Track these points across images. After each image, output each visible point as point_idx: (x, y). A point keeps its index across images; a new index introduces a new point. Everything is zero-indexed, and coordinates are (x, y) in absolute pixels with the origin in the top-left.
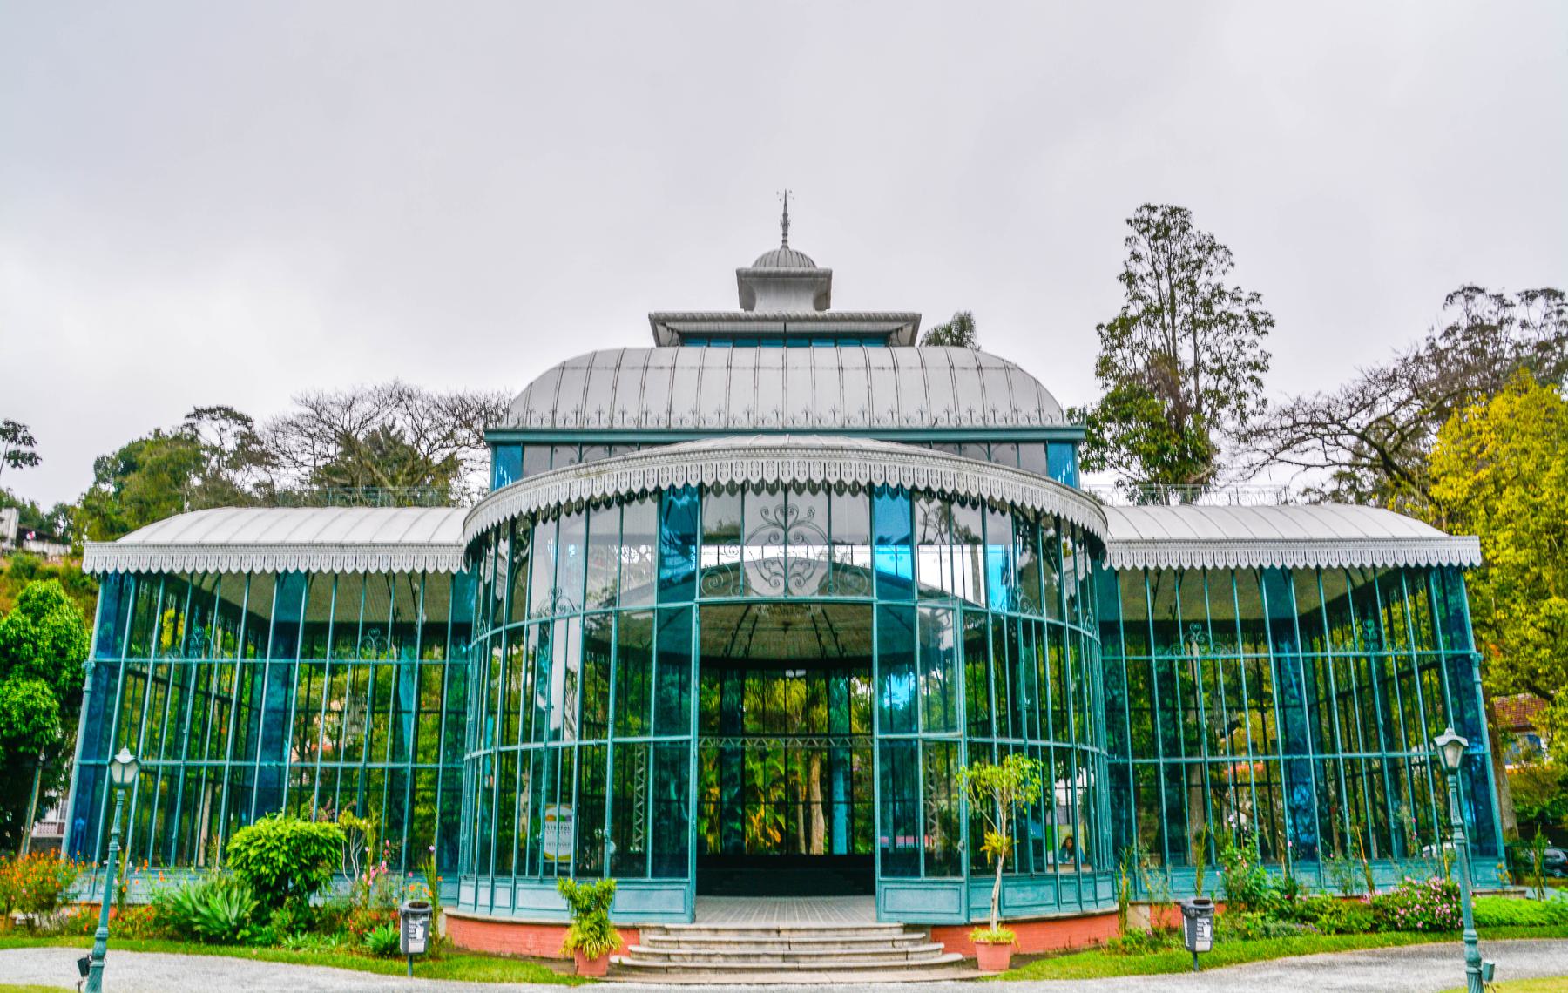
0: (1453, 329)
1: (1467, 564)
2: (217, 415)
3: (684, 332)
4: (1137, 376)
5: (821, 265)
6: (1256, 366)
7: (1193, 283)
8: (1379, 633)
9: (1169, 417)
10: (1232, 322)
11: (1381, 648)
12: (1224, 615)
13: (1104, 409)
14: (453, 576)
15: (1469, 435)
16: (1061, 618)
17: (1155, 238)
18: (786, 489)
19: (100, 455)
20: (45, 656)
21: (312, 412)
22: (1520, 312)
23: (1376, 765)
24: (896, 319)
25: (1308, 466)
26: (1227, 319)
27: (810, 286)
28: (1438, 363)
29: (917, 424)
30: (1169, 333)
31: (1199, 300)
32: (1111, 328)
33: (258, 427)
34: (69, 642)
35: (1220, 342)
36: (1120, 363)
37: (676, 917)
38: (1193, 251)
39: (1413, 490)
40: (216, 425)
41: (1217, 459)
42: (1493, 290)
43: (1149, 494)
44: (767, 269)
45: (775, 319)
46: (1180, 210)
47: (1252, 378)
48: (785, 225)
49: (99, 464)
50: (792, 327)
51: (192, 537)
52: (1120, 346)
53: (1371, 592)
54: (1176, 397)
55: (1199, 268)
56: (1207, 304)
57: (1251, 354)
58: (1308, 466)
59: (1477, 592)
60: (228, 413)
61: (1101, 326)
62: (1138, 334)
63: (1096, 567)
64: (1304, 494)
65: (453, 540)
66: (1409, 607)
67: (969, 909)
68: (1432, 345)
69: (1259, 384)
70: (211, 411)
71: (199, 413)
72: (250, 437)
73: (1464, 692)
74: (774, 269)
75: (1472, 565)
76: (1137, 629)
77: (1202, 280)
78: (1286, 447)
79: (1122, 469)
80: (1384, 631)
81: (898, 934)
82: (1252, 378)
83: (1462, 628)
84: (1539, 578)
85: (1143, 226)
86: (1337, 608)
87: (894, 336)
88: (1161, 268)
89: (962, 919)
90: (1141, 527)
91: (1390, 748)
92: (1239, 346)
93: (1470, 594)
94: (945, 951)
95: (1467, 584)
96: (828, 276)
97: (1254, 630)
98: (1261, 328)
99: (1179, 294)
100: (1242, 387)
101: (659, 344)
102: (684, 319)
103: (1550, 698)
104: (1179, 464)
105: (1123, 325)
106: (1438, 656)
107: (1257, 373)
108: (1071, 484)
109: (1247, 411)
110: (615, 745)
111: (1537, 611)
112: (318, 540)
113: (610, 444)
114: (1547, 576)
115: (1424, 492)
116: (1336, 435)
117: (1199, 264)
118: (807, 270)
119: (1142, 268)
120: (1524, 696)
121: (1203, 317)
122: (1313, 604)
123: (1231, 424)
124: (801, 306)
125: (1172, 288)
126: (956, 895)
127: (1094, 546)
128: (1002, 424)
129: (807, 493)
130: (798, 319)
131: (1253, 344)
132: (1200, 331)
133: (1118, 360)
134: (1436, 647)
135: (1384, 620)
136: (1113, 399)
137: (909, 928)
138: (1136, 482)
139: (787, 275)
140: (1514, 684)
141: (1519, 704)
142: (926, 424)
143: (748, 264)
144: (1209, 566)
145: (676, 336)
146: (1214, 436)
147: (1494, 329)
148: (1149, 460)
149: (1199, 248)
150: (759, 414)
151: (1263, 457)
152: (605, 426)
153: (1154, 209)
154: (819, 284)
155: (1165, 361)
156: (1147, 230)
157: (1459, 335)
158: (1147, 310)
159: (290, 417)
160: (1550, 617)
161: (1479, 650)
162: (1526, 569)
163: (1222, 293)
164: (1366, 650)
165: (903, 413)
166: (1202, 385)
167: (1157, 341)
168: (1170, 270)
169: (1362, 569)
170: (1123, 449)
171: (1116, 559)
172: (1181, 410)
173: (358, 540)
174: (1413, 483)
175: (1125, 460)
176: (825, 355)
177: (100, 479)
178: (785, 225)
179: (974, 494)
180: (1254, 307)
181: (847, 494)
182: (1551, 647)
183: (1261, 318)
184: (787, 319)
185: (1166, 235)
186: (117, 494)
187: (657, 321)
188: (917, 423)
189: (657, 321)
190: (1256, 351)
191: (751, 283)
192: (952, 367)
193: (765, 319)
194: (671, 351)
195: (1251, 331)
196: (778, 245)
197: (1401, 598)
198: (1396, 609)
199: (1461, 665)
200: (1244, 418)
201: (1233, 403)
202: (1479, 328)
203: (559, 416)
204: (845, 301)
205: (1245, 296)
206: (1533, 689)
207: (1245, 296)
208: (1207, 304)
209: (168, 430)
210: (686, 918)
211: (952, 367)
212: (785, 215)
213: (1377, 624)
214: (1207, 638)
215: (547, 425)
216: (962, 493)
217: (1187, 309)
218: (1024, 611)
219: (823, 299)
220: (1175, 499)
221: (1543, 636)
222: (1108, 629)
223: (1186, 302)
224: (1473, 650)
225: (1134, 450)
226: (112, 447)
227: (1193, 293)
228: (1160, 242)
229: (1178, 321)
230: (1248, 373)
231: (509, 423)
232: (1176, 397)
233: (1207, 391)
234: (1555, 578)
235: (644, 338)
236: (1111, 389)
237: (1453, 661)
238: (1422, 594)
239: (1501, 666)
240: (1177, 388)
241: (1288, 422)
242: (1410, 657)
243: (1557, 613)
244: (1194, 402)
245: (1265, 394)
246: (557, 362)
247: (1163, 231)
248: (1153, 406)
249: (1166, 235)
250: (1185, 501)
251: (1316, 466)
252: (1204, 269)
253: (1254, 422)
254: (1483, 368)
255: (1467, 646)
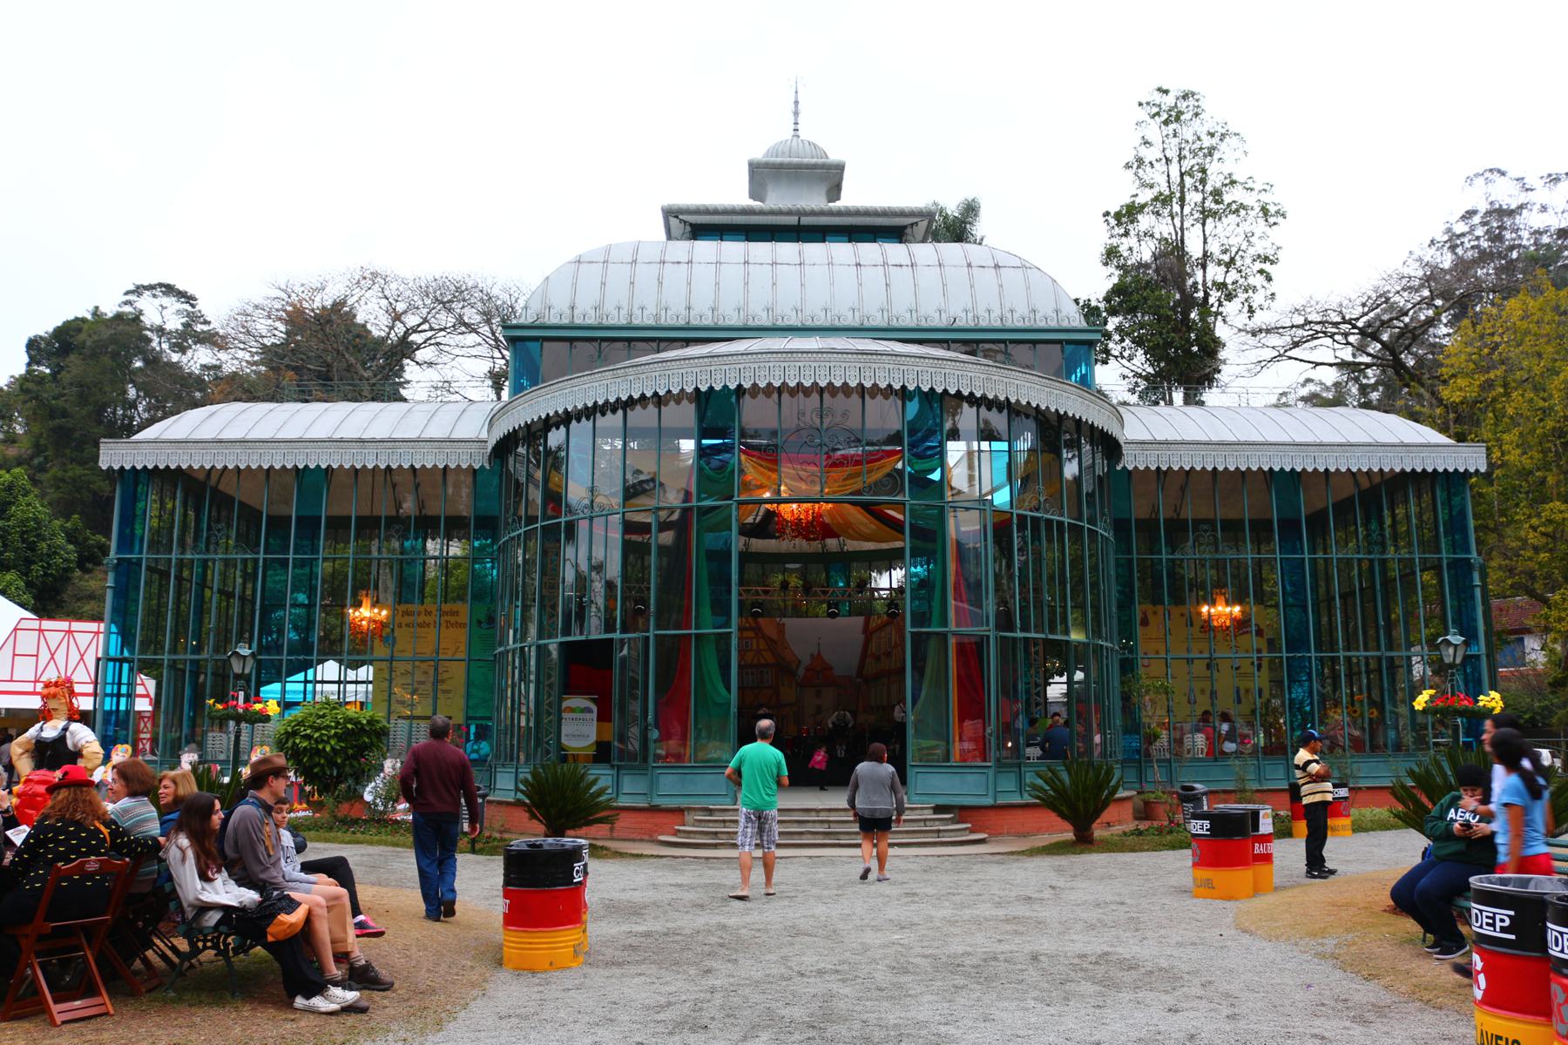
0: (1471, 213)
1: (1472, 470)
2: (158, 292)
3: (702, 226)
4: (1141, 265)
5: (834, 157)
6: (1266, 259)
7: (1204, 171)
8: (1383, 536)
9: (1173, 309)
10: (1242, 212)
11: (1384, 552)
12: (1232, 515)
13: (1107, 299)
14: (475, 471)
15: (1482, 337)
16: (1080, 518)
17: (1166, 123)
18: (821, 391)
19: (32, 335)
20: (16, 550)
21: (284, 296)
22: (1541, 195)
23: (1373, 665)
24: (912, 214)
25: (1318, 364)
26: (1238, 209)
27: (822, 179)
28: (1453, 248)
29: (936, 323)
30: (1177, 221)
31: (1209, 188)
32: (1118, 216)
33: (203, 306)
34: (38, 536)
35: (1226, 232)
36: (1125, 254)
37: (720, 799)
38: (1205, 138)
39: (1422, 390)
40: (157, 302)
41: (1222, 355)
42: (1513, 173)
43: (1154, 389)
44: (779, 160)
45: (789, 213)
46: (1193, 94)
47: (1261, 272)
48: (796, 114)
49: (33, 345)
50: (805, 221)
51: (207, 433)
52: (1126, 234)
53: (1377, 494)
54: (1182, 291)
55: (1211, 155)
56: (1217, 194)
57: (1260, 247)
58: (1318, 364)
59: (1481, 495)
60: (169, 290)
61: (1107, 214)
62: (1145, 221)
63: (1112, 466)
64: (1303, 385)
65: (471, 435)
66: (1413, 509)
67: (996, 792)
68: (1449, 230)
69: (1269, 279)
70: (151, 287)
71: (139, 290)
72: (193, 318)
73: (1463, 592)
74: (787, 160)
75: (1477, 471)
76: (1148, 527)
77: (1213, 168)
78: (1296, 345)
79: (1124, 362)
80: (1388, 532)
81: (929, 815)
82: (1261, 272)
83: (1464, 529)
84: (1543, 481)
85: (1155, 110)
86: (1343, 508)
87: (908, 231)
88: (1172, 153)
89: (989, 801)
90: (1160, 430)
91: (1390, 647)
92: (1248, 237)
93: (1473, 497)
94: (972, 831)
95: (1472, 487)
96: (840, 168)
97: (1261, 529)
98: (1272, 220)
99: (1188, 181)
100: (1252, 281)
101: (670, 237)
102: (697, 211)
103: (1545, 601)
104: (1185, 361)
105: (1129, 214)
106: (1440, 559)
107: (1267, 267)
108: (1086, 383)
109: (1255, 305)
110: (656, 636)
111: (1538, 515)
112: (337, 436)
113: (629, 340)
114: (1551, 480)
115: (1433, 393)
116: (1346, 335)
117: (1211, 151)
118: (821, 161)
119: (1150, 154)
120: (1521, 599)
121: (1213, 206)
122: (1320, 506)
123: (1241, 320)
124: (811, 200)
125: (1182, 175)
126: (983, 778)
127: (1109, 446)
128: (1020, 325)
129: (840, 395)
130: (813, 213)
131: (1263, 237)
132: (1209, 221)
133: (1123, 250)
134: (1438, 551)
135: (1388, 521)
136: (1117, 290)
137: (938, 809)
138: (1140, 376)
139: (790, 166)
140: (1512, 586)
141: (1516, 607)
142: (944, 323)
143: (759, 154)
144: (1221, 468)
145: (688, 229)
146: (1221, 331)
147: (1511, 213)
148: (1154, 353)
149: (1212, 135)
150: (778, 311)
151: (1269, 354)
152: (623, 322)
153: (1166, 92)
154: (831, 176)
155: (1173, 253)
156: (1158, 114)
157: (1476, 219)
158: (1156, 199)
159: (259, 301)
160: (1550, 521)
161: (1479, 554)
162: (1531, 472)
163: (1233, 182)
164: (1370, 553)
165: (922, 312)
166: (1209, 278)
167: (1164, 228)
168: (1181, 158)
169: (1369, 473)
170: (1127, 342)
171: (1130, 461)
172: (1188, 302)
173: (378, 436)
174: (1423, 385)
175: (1126, 354)
176: (842, 251)
177: (33, 360)
178: (796, 114)
179: (1002, 398)
180: (1265, 198)
181: (879, 397)
182: (1550, 551)
183: (1272, 209)
184: (801, 213)
185: (1177, 119)
186: (54, 375)
187: (670, 213)
188: (936, 322)
189: (670, 213)
190: (1267, 244)
191: (762, 174)
192: (969, 265)
193: (780, 213)
194: (686, 244)
195: (1261, 221)
196: (789, 134)
197: (1406, 501)
198: (1400, 511)
199: (1462, 569)
200: (1251, 311)
201: (1242, 296)
202: (1501, 213)
203: (576, 312)
204: (857, 195)
205: (1258, 187)
206: (1531, 593)
207: (1258, 187)
208: (1217, 194)
209: (109, 309)
210: (728, 800)
211: (969, 265)
212: (796, 103)
213: (1382, 529)
214: (1215, 538)
215: (565, 321)
216: (991, 397)
217: (1198, 197)
218: (1047, 512)
219: (835, 191)
220: (1178, 396)
221: (1544, 540)
222: (1121, 526)
223: (1196, 189)
224: (1474, 554)
225: (1139, 342)
226: (45, 325)
227: (1203, 181)
228: (1173, 126)
229: (1187, 210)
230: (1258, 266)
231: (527, 319)
232: (1182, 291)
233: (1214, 283)
234: (1558, 483)
235: (655, 229)
236: (1115, 280)
237: (1453, 564)
238: (1426, 497)
239: (1500, 567)
240: (1184, 281)
241: (1300, 320)
242: (1412, 560)
243: (1558, 517)
244: (1201, 294)
245: (1273, 287)
246: (572, 257)
247: (1174, 117)
248: (1160, 298)
249: (1177, 119)
250: (1188, 401)
251: (1324, 361)
252: (1217, 155)
253: (1261, 319)
254: (1500, 256)
255: (1468, 551)
